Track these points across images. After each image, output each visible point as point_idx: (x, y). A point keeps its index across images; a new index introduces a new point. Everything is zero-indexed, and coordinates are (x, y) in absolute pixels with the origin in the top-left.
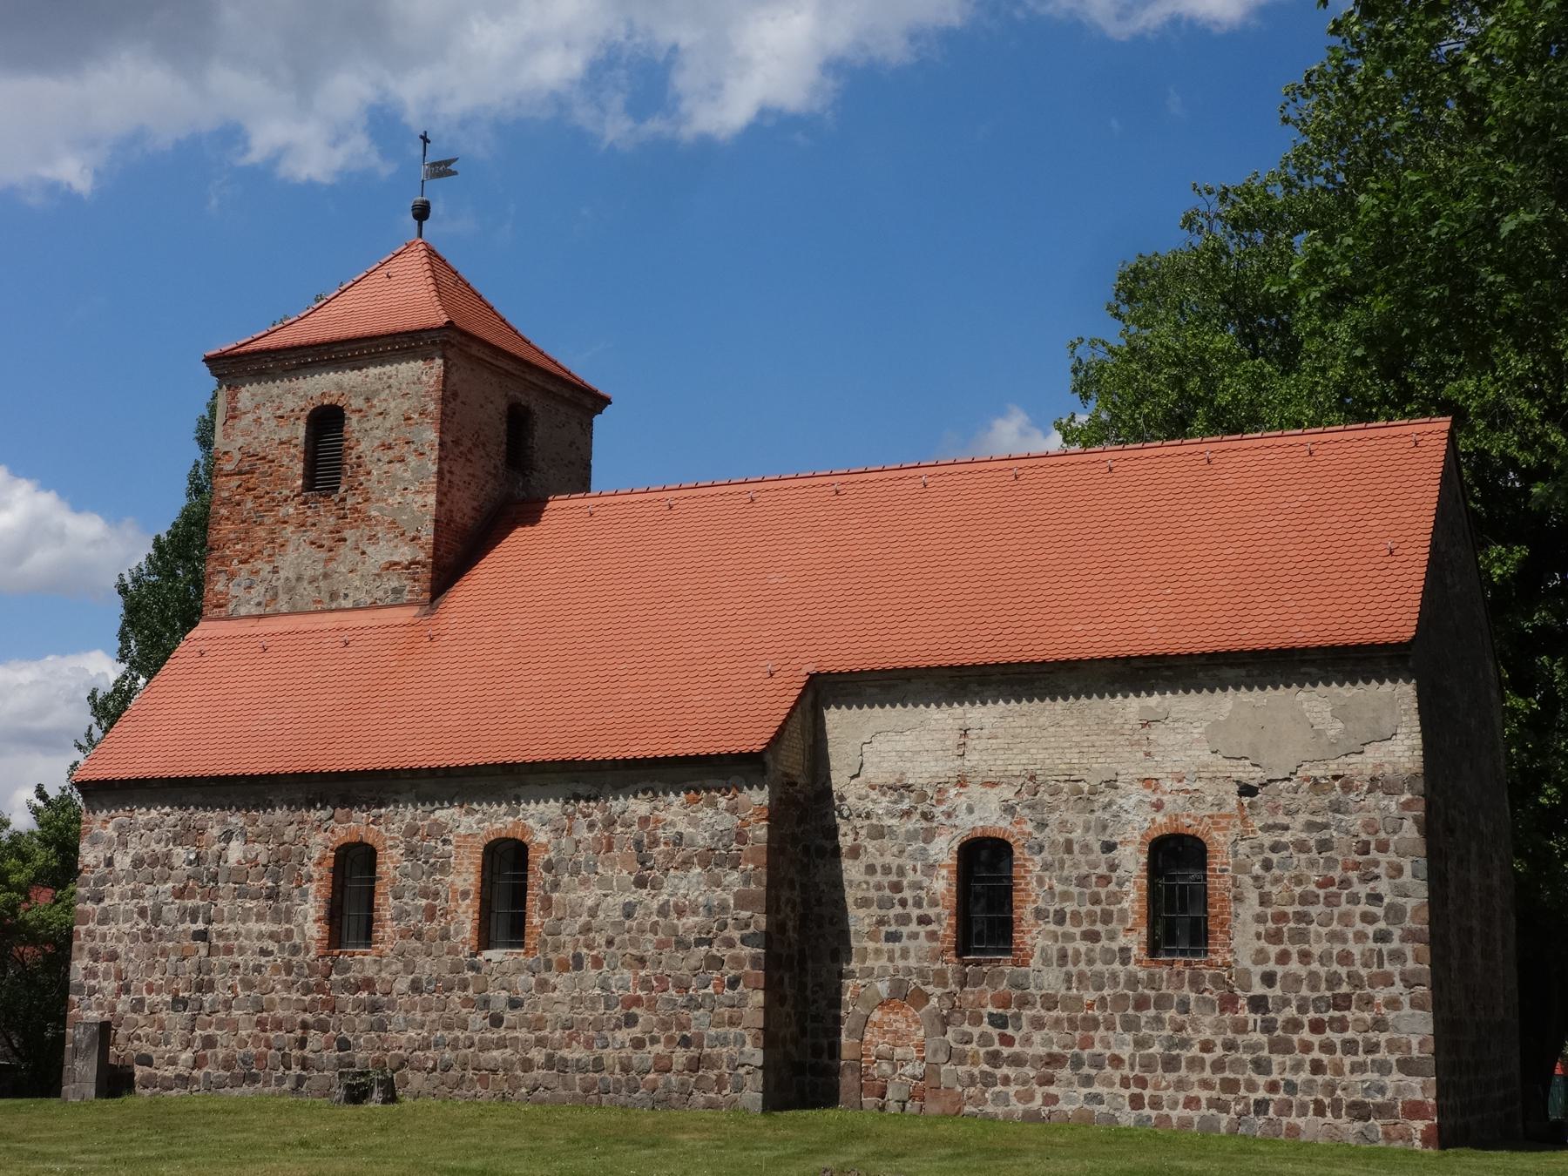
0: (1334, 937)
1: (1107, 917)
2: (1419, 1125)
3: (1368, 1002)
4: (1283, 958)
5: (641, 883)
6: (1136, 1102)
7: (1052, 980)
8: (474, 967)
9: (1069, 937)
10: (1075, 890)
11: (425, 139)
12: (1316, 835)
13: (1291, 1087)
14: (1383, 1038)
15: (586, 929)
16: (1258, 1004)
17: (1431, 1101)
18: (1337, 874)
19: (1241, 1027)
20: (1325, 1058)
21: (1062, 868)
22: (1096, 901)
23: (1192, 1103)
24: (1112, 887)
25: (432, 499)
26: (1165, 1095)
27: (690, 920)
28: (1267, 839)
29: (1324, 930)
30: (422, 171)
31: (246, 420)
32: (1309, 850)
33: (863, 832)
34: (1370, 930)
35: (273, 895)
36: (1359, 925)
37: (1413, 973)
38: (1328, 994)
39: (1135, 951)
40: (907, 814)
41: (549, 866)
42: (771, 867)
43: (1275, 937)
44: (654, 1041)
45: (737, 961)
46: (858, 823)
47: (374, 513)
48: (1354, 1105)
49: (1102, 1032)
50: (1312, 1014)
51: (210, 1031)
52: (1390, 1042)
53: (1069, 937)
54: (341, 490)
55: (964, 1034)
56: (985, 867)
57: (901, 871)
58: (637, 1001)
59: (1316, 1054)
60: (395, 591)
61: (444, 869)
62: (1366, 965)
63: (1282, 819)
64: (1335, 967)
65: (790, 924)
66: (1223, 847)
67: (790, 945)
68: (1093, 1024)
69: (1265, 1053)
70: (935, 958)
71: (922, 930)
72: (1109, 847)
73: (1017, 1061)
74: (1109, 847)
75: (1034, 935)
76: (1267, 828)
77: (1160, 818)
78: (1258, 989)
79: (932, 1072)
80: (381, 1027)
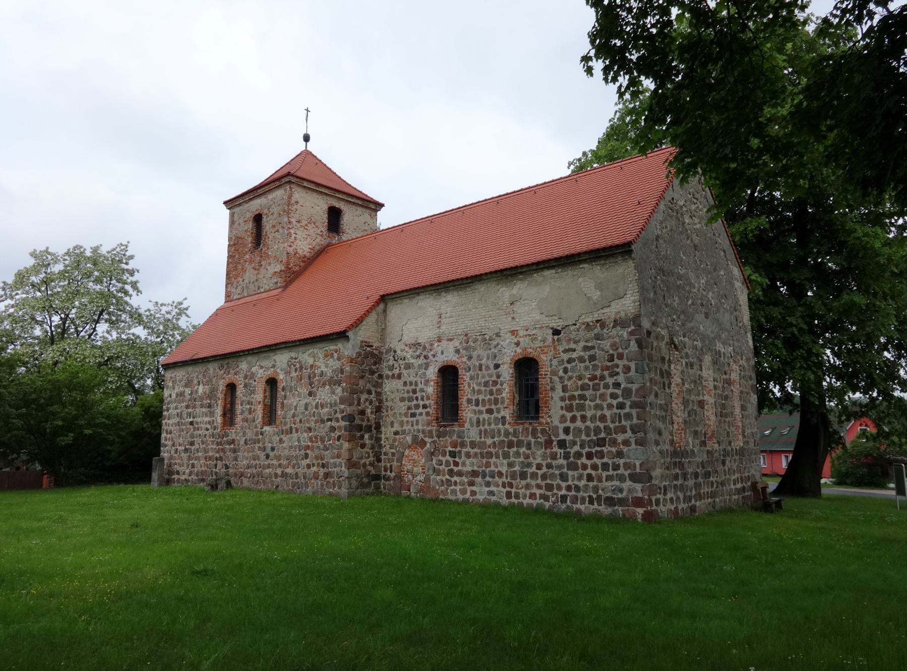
0: (597, 407)
1: (496, 401)
3: (614, 442)
4: (573, 419)
5: (310, 394)
8: (262, 434)
9: (481, 412)
10: (483, 389)
11: (307, 110)
12: (588, 353)
13: (577, 489)
14: (622, 461)
16: (562, 444)
18: (598, 373)
19: (554, 457)
20: (593, 473)
23: (533, 496)
24: (499, 386)
27: (326, 410)
28: (565, 357)
29: (592, 404)
32: (585, 361)
33: (402, 367)
34: (615, 402)
36: (609, 400)
38: (595, 438)
39: (508, 418)
40: (419, 356)
43: (569, 409)
45: (340, 428)
46: (401, 362)
49: (494, 460)
50: (587, 449)
52: (625, 464)
53: (481, 412)
57: (416, 385)
58: (308, 447)
59: (589, 471)
62: (613, 422)
63: (572, 346)
64: (598, 423)
65: (369, 411)
67: (368, 420)
69: (565, 470)
70: (428, 425)
71: (424, 411)
72: (497, 366)
73: (460, 474)
75: (467, 413)
76: (565, 351)
77: (519, 350)
78: (562, 436)
79: (427, 479)
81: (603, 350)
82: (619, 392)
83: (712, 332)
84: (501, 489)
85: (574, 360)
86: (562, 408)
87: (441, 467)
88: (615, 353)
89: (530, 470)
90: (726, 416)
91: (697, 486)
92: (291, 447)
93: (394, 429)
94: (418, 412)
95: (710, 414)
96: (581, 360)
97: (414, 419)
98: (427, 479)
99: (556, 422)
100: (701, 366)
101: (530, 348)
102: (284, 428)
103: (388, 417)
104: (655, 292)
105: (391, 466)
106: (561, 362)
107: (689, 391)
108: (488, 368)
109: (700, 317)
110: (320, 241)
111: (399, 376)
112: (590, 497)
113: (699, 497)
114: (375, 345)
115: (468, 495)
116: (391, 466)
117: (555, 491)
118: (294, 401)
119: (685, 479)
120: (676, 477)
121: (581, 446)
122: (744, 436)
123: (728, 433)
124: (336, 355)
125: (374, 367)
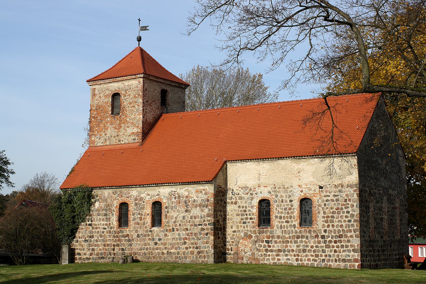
0: (339, 221)
1: (291, 217)
2: (357, 264)
3: (346, 236)
4: (328, 226)
5: (186, 211)
6: (297, 260)
7: (278, 232)
8: (151, 231)
9: (282, 222)
10: (284, 211)
11: (139, 20)
12: (336, 198)
13: (330, 256)
14: (349, 244)
15: (175, 222)
16: (323, 237)
17: (359, 258)
18: (340, 207)
19: (319, 242)
20: (337, 249)
21: (281, 206)
22: (288, 213)
23: (309, 260)
24: (292, 210)
25: (141, 116)
26: (303, 258)
27: (197, 220)
28: (325, 199)
29: (337, 220)
30: (139, 28)
31: (97, 97)
32: (334, 201)
33: (237, 198)
34: (347, 220)
35: (106, 215)
36: (345, 219)
37: (356, 229)
38: (338, 234)
39: (297, 225)
40: (247, 194)
41: (166, 208)
42: (215, 207)
43: (327, 222)
44: (190, 247)
45: (207, 229)
46: (236, 196)
47: (128, 120)
48: (343, 259)
49: (290, 244)
50: (334, 239)
51: (93, 247)
52: (351, 245)
53: (282, 222)
54: (120, 114)
55: (260, 245)
56: (264, 206)
57: (246, 207)
58: (186, 239)
59: (335, 248)
60: (134, 139)
61: (143, 208)
62: (346, 228)
63: (328, 194)
64: (340, 228)
65: (220, 221)
66: (316, 200)
67: (220, 225)
68: (288, 242)
69: (324, 248)
70: (254, 227)
71: (251, 221)
72: (291, 201)
73: (271, 251)
74: (291, 201)
75: (275, 222)
76: (325, 196)
77: (302, 194)
78: (323, 234)
79: (253, 254)
80: (131, 245)
81: (342, 197)
82: (349, 215)
83: (388, 185)
84: (293, 257)
85: (329, 201)
86: (323, 221)
87: (261, 248)
88: (348, 199)
89: (308, 249)
90: (393, 224)
91: (379, 255)
92: (173, 239)
93: (233, 229)
94: (247, 221)
95: (385, 224)
96: (333, 201)
97: (245, 225)
98: (253, 254)
99: (320, 227)
100: (382, 202)
101: (308, 194)
102: (168, 228)
103: (229, 224)
104: (364, 172)
105: (231, 248)
106: (323, 201)
107: (377, 214)
108: (286, 201)
109: (382, 179)
110: (158, 112)
111: (236, 203)
112: (335, 259)
113: (379, 260)
114: (223, 187)
115: (276, 261)
116: (231, 248)
117: (320, 257)
118: (173, 215)
119: (374, 252)
120: (371, 251)
121: (331, 238)
122: (401, 234)
123: (393, 232)
124: (204, 192)
125: (222, 198)
